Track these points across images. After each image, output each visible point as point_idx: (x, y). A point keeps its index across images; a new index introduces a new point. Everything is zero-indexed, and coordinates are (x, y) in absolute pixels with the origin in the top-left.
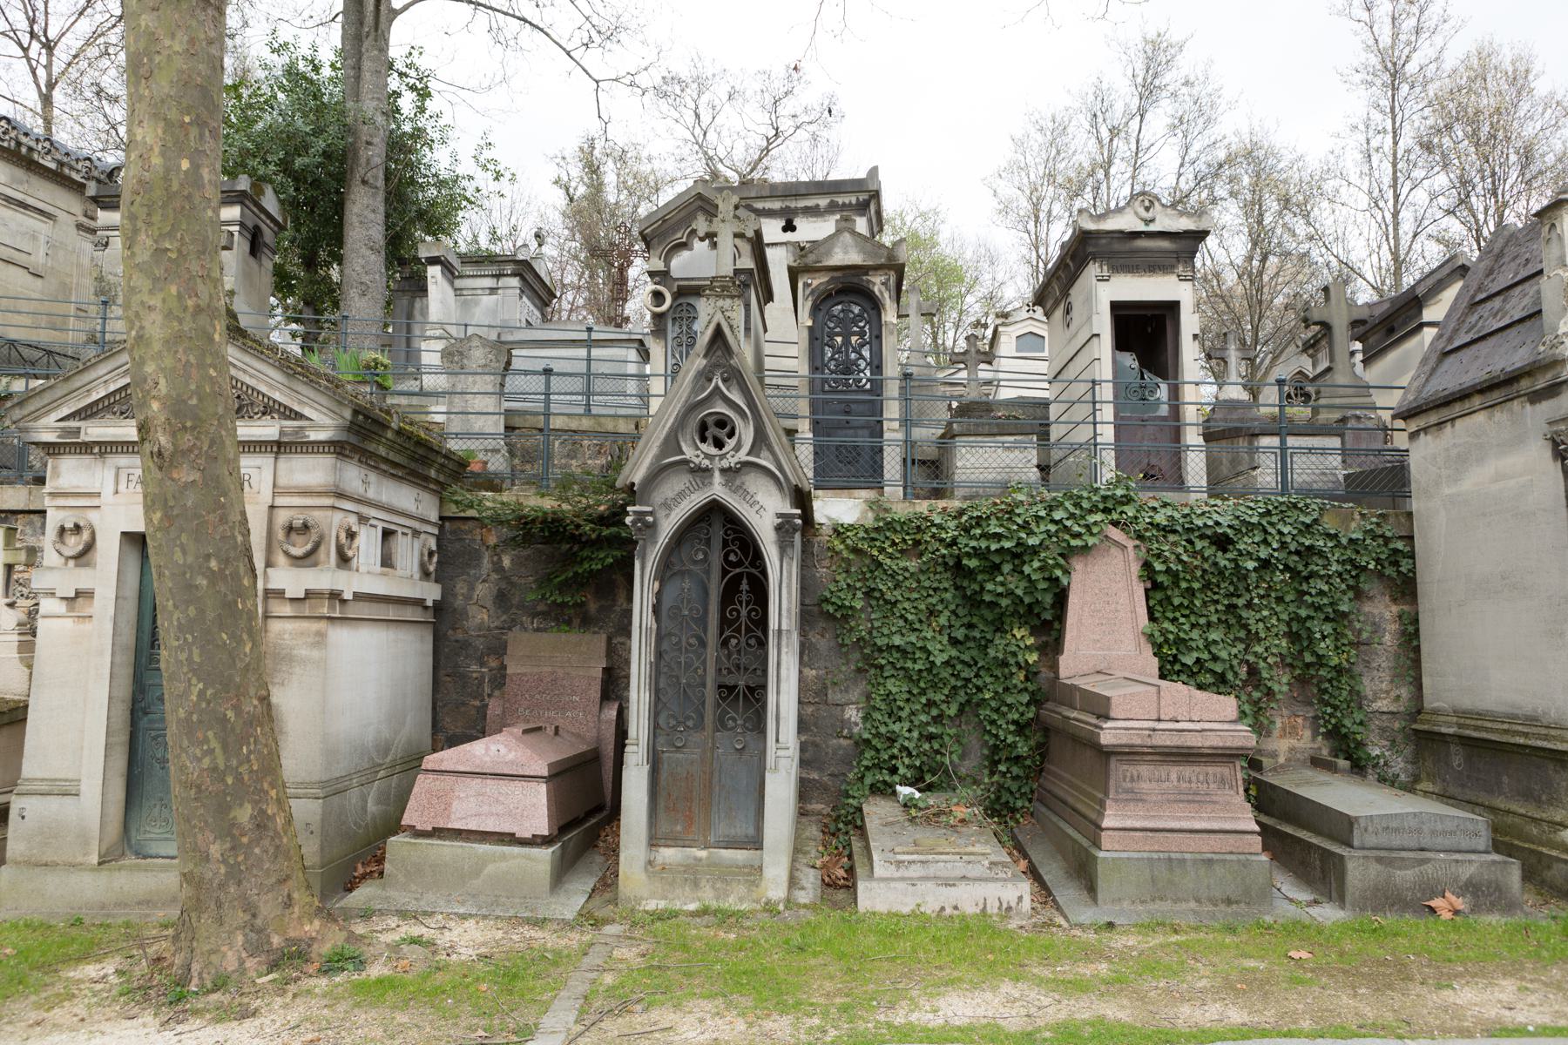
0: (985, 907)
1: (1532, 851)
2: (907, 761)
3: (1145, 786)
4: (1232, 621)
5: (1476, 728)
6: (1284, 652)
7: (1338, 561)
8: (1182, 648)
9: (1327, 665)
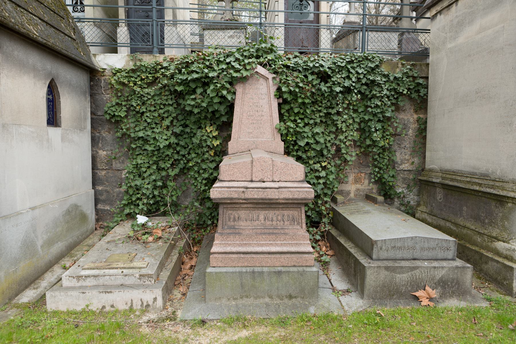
0: (132, 305)
1: (477, 252)
2: (145, 201)
3: (242, 224)
4: (329, 122)
5: (452, 180)
6: (356, 139)
7: (387, 89)
8: (299, 137)
9: (377, 146)
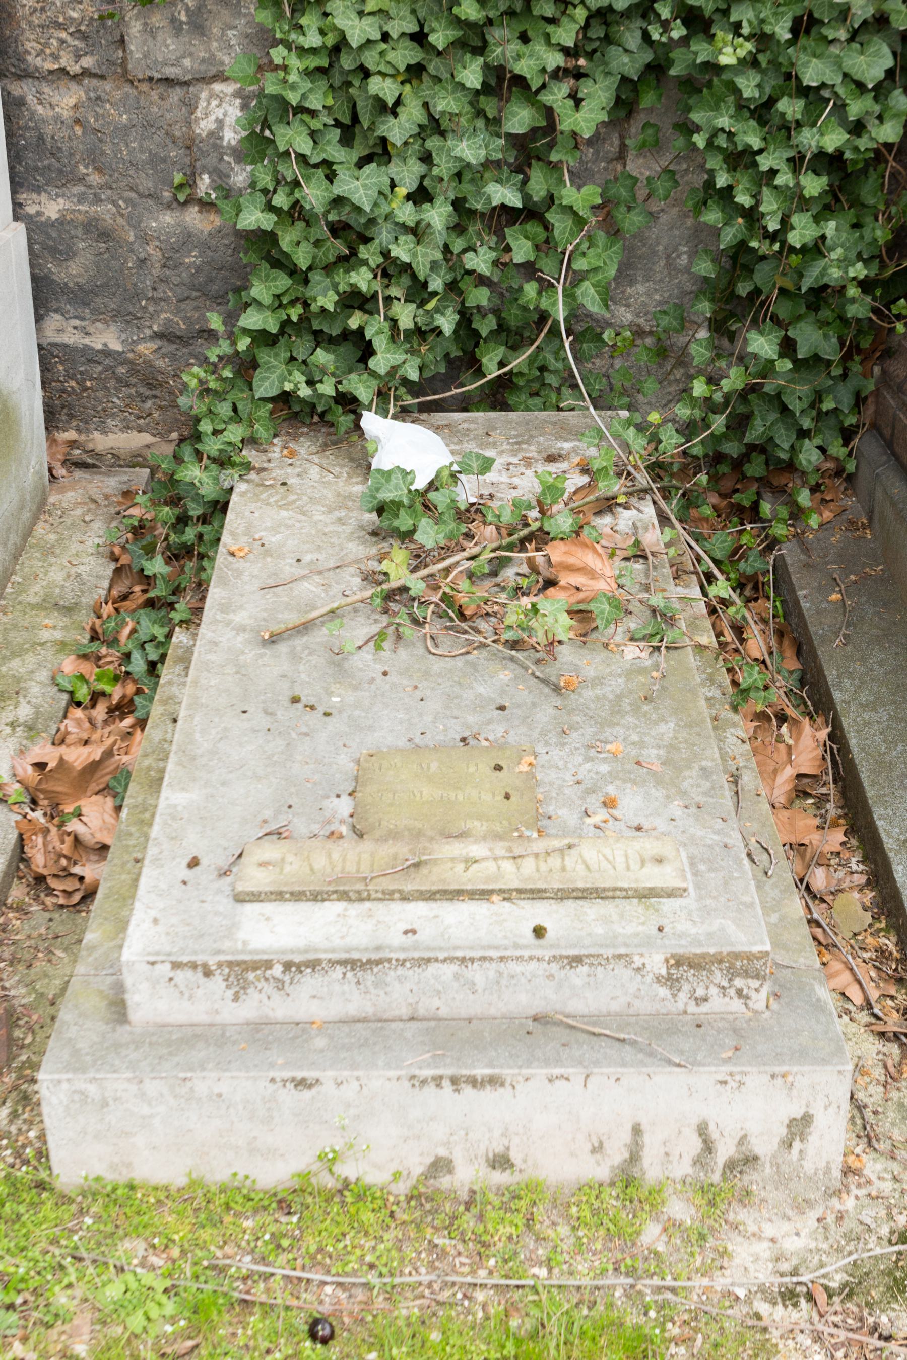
0: (634, 1157)
